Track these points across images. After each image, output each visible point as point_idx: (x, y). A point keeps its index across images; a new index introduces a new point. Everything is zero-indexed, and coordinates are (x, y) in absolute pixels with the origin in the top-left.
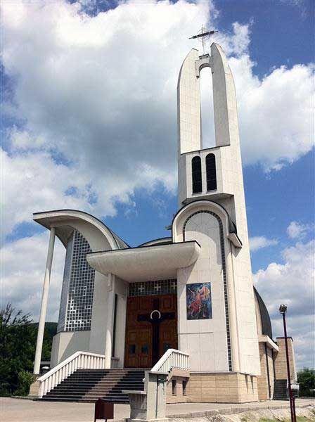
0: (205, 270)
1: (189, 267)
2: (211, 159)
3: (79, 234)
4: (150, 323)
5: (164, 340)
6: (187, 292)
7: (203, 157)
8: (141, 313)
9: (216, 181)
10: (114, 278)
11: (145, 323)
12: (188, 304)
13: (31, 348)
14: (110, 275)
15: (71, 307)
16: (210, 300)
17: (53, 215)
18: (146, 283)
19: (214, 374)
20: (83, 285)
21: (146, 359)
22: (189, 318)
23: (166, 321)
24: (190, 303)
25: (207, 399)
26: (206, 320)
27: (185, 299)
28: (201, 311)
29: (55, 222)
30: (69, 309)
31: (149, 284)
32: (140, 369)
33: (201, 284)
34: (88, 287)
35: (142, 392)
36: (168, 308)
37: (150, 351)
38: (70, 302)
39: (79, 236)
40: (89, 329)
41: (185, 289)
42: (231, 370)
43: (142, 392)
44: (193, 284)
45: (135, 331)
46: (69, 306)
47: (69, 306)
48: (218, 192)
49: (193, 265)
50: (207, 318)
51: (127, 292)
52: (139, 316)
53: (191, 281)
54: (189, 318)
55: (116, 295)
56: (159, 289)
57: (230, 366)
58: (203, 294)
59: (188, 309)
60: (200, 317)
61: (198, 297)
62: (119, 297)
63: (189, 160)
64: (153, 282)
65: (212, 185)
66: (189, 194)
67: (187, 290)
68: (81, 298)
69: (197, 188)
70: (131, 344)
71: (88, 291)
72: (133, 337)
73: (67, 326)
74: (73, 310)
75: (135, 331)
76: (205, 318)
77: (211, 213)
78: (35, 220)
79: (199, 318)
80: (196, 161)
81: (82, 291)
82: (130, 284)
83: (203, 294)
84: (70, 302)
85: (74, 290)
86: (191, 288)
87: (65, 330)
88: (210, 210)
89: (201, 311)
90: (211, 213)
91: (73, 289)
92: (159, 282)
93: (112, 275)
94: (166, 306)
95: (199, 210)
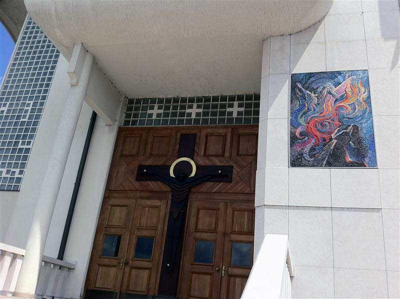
5: (197, 230)
10: (88, 61)
11: (153, 185)
12: (294, 124)
13: (245, 248)
14: (77, 50)
16: (368, 113)
18: (168, 101)
20: (25, 98)
21: (145, 274)
22: (296, 161)
23: (209, 184)
24: (302, 121)
33: (339, 73)
37: (158, 252)
44: (311, 75)
45: (125, 202)
49: (314, 27)
50: (360, 165)
51: (120, 117)
52: (141, 167)
53: (307, 64)
54: (296, 161)
55: (94, 116)
58: (344, 97)
59: (293, 139)
60: (335, 160)
61: (329, 107)
62: (101, 123)
67: (293, 88)
70: (113, 231)
72: (118, 216)
75: (125, 202)
79: (329, 165)
82: (131, 101)
93: (85, 50)
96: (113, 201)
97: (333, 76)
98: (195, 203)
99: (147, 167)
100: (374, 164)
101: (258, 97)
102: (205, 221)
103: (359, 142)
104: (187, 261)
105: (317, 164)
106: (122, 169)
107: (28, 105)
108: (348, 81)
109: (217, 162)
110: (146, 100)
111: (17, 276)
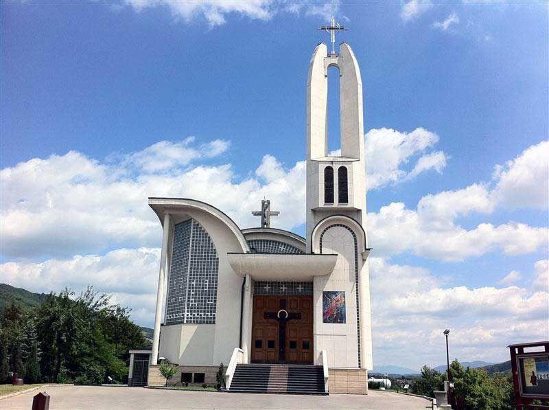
0: (339, 281)
1: (327, 276)
2: (343, 172)
3: (198, 225)
4: (276, 322)
5: (290, 337)
6: (324, 300)
7: (336, 168)
8: (269, 311)
9: (347, 194)
11: (272, 321)
12: (324, 309)
15: (191, 299)
16: (344, 307)
17: (173, 203)
18: (272, 282)
19: (346, 370)
21: (273, 354)
25: (340, 390)
26: (340, 324)
27: (322, 305)
28: (335, 316)
29: (170, 208)
30: (189, 301)
31: (275, 284)
32: (268, 365)
34: (209, 281)
35: (193, 375)
36: (295, 309)
37: (277, 346)
38: (189, 295)
39: (197, 227)
40: (214, 323)
41: (322, 295)
42: (360, 367)
43: (193, 375)
44: (328, 292)
46: (189, 298)
47: (189, 298)
48: (349, 205)
53: (327, 288)
56: (269, 289)
57: (359, 364)
58: (338, 301)
60: (335, 321)
63: (322, 168)
64: (279, 283)
65: (344, 198)
66: (321, 203)
67: (324, 296)
68: (203, 291)
69: (329, 198)
71: (209, 285)
72: (259, 333)
73: (187, 318)
74: (193, 303)
75: (261, 327)
76: (338, 323)
77: (347, 227)
78: (151, 205)
79: (334, 322)
80: (329, 171)
81: (203, 285)
82: (256, 282)
83: (338, 301)
84: (189, 295)
85: (194, 283)
86: (327, 295)
87: (185, 322)
88: (354, 231)
89: (335, 316)
90: (351, 231)
91: (193, 281)
92: (286, 283)
94: (292, 307)
95: (338, 223)
96: (256, 327)
97: (335, 293)
98: (289, 327)
99: (269, 313)
100: (345, 322)
101: (312, 283)
102: (293, 334)
103: (342, 315)
104: (288, 348)
105: (330, 322)
106: (258, 314)
107: (206, 282)
108: (339, 295)
109: (295, 311)
110: (263, 282)
111: (162, 286)
